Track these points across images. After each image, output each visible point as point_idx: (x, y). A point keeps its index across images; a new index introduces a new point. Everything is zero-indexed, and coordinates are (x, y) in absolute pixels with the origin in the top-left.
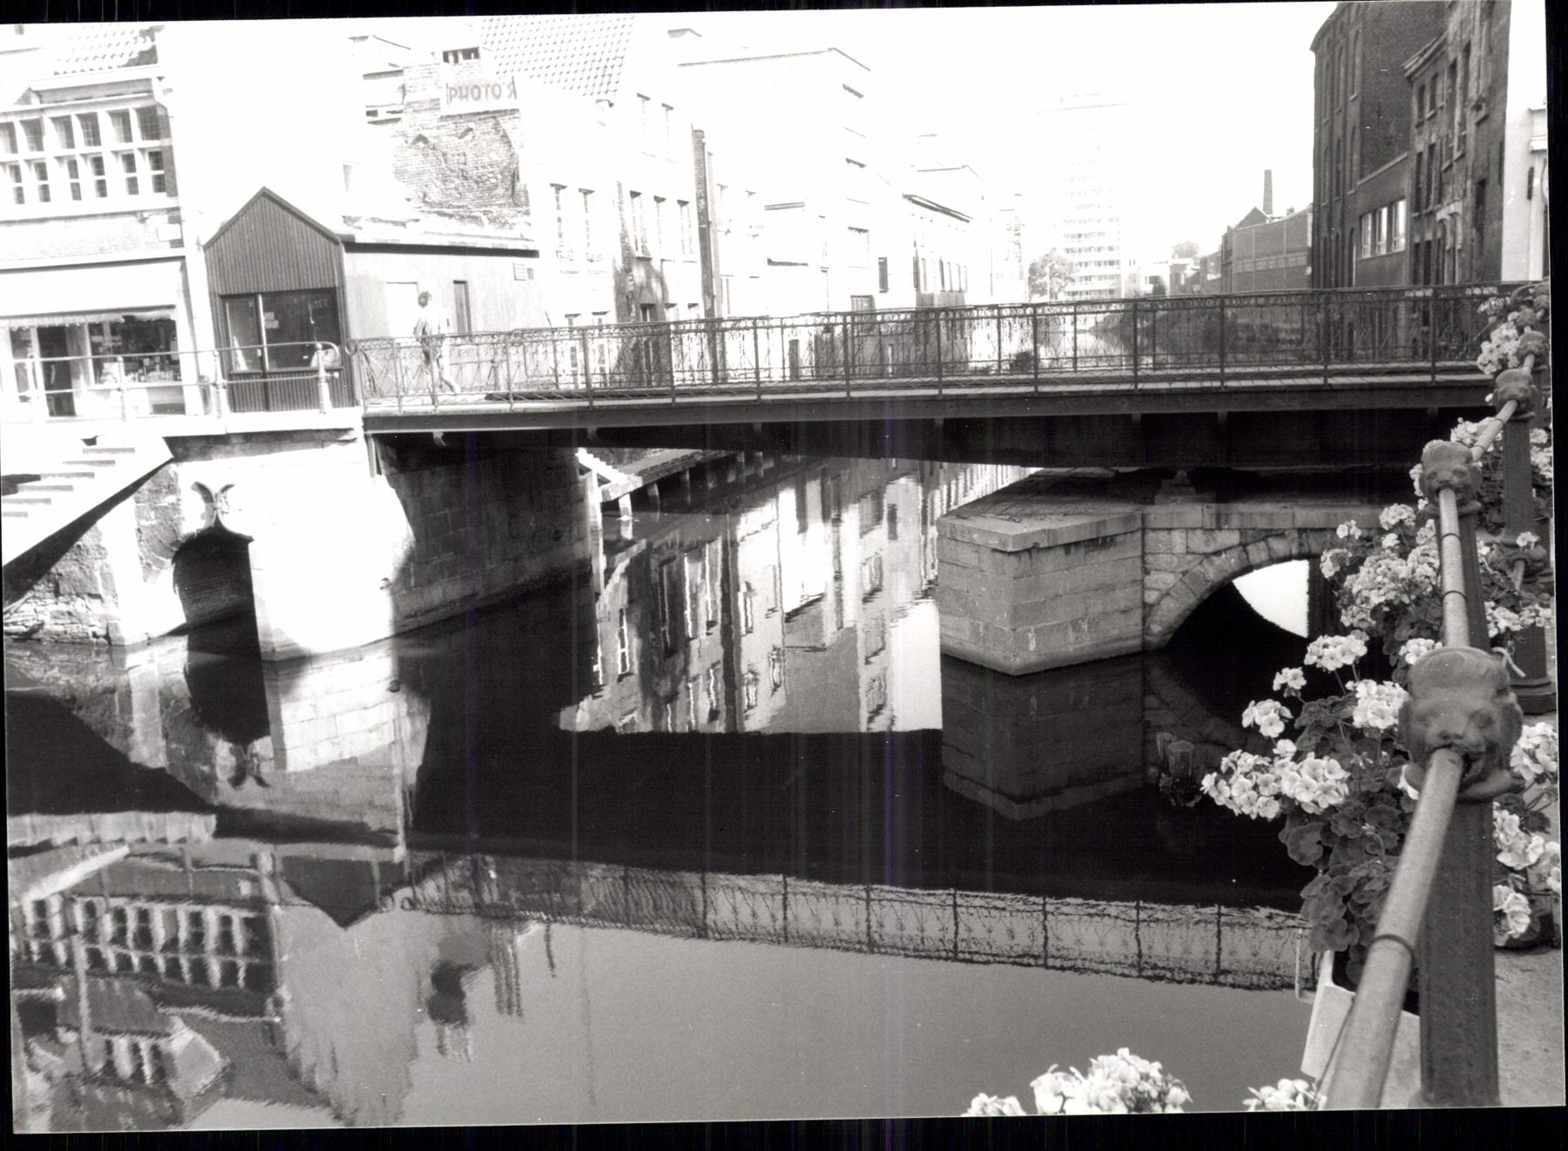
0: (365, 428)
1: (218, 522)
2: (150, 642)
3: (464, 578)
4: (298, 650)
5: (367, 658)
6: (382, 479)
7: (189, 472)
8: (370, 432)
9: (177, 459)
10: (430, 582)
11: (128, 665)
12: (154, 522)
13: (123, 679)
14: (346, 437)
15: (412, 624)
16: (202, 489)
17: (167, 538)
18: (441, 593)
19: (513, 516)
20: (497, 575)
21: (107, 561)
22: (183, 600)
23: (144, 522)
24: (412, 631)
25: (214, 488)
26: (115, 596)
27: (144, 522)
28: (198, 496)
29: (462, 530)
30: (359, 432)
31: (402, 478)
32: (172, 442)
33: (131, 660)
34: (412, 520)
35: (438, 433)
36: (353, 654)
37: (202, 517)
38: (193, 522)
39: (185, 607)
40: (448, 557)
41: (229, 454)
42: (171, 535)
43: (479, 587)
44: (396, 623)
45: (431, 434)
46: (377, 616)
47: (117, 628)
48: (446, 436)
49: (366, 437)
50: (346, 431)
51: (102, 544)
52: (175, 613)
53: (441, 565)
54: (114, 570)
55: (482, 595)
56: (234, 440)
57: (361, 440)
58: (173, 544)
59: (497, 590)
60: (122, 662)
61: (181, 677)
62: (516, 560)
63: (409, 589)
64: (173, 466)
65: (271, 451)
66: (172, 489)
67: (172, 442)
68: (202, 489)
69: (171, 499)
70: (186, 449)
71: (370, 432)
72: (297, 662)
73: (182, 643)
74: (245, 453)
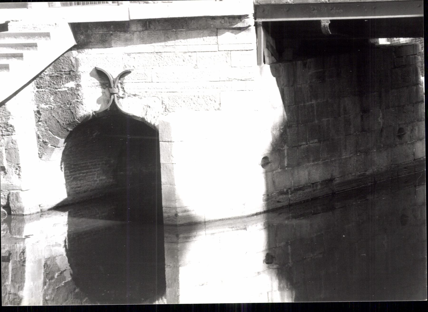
0: (256, 16)
1: (114, 104)
2: (42, 213)
3: (326, 164)
4: (189, 217)
5: (250, 228)
6: (267, 68)
7: (91, 58)
8: (260, 20)
9: (80, 46)
10: (299, 165)
11: (25, 234)
12: (53, 105)
13: (19, 246)
14: (240, 25)
15: (284, 200)
16: (101, 75)
17: (63, 118)
18: (310, 174)
19: (365, 111)
20: (350, 165)
21: (13, 137)
22: (67, 177)
23: (43, 106)
24: (280, 209)
25: (113, 73)
26: (18, 168)
27: (43, 106)
28: (96, 81)
29: (325, 120)
30: (250, 21)
31: (282, 67)
32: (77, 28)
33: (28, 228)
34: (287, 106)
35: (325, 21)
36: (240, 221)
37: (98, 102)
38: (91, 102)
39: (68, 183)
40: (313, 143)
41: (128, 42)
42: (69, 117)
43: (336, 174)
44: (269, 198)
45: (319, 22)
46: (252, 191)
47: (17, 198)
48: (333, 22)
49: (256, 25)
50: (240, 18)
51: (10, 122)
52: (58, 189)
53: (308, 150)
54: (19, 146)
55: (338, 181)
56: (133, 28)
57: (253, 28)
58: (69, 125)
59: (350, 178)
60: (20, 231)
61: (62, 251)
62: (367, 152)
63: (283, 168)
64: (75, 53)
65: (167, 38)
66: (72, 75)
67: (77, 28)
68: (101, 75)
69: (71, 84)
70: (88, 36)
71: (260, 20)
72: (190, 226)
73: (63, 218)
74: (143, 41)
